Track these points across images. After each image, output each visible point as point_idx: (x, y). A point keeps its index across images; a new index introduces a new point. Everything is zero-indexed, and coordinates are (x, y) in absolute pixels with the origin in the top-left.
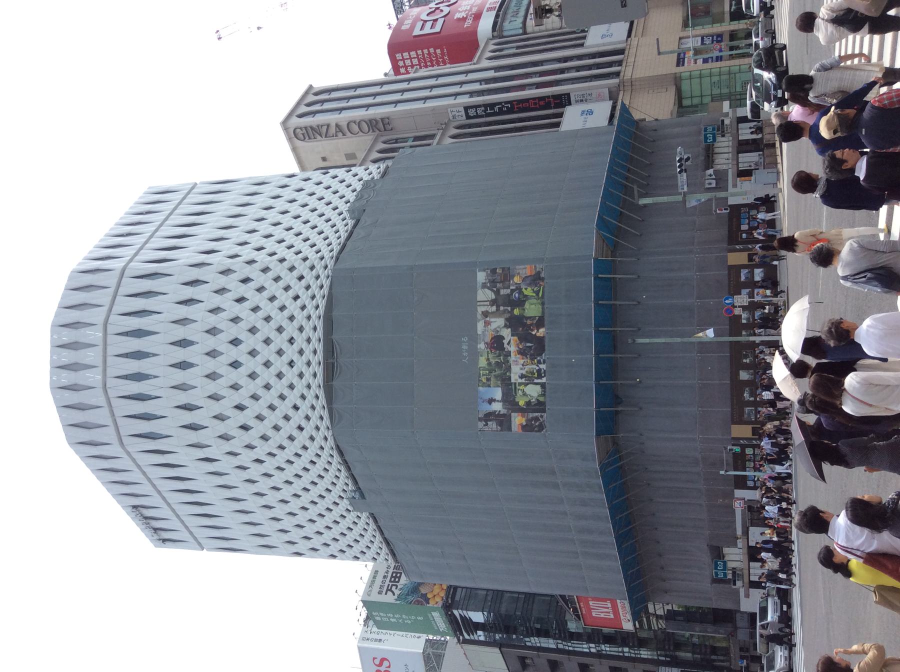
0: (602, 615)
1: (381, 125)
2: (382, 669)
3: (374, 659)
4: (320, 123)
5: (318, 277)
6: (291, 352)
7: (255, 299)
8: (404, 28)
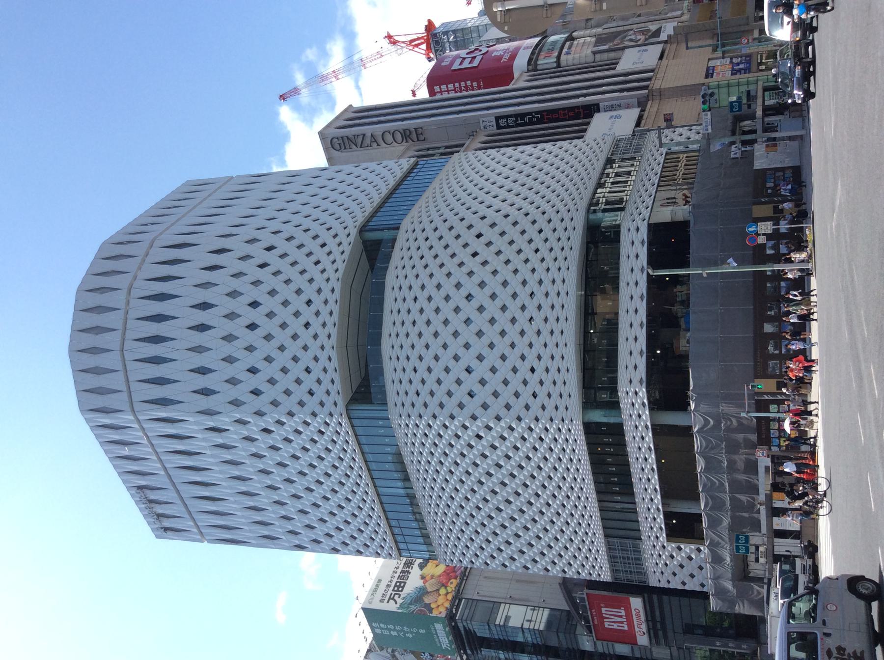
0: (615, 626)
1: (414, 136)
4: (357, 133)
8: (443, 64)
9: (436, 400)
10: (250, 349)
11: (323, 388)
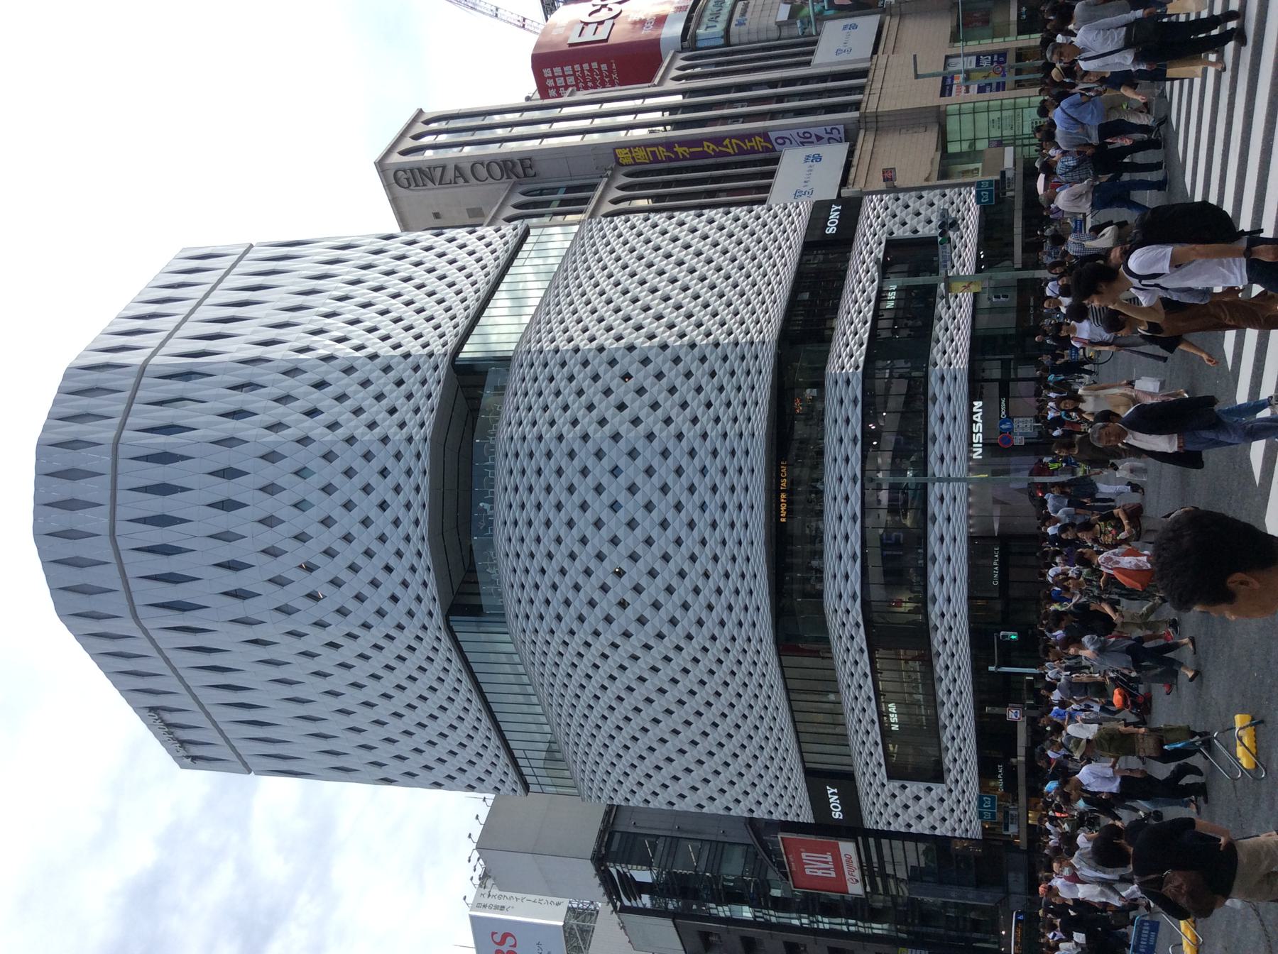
0: (820, 873)
1: (519, 169)
2: (505, 948)
3: (493, 934)
5: (417, 411)
6: (382, 522)
7: (334, 411)
9: (569, 581)
10: (301, 538)
11: (411, 592)
